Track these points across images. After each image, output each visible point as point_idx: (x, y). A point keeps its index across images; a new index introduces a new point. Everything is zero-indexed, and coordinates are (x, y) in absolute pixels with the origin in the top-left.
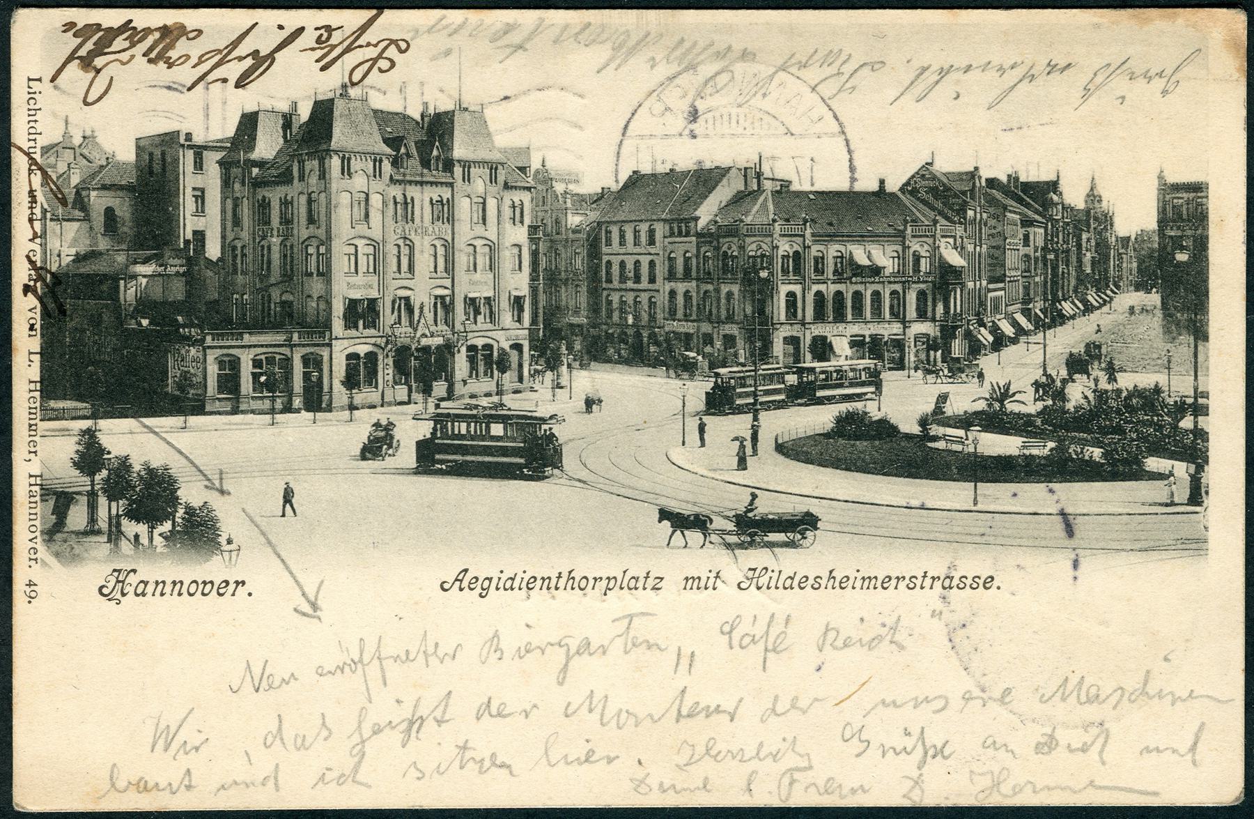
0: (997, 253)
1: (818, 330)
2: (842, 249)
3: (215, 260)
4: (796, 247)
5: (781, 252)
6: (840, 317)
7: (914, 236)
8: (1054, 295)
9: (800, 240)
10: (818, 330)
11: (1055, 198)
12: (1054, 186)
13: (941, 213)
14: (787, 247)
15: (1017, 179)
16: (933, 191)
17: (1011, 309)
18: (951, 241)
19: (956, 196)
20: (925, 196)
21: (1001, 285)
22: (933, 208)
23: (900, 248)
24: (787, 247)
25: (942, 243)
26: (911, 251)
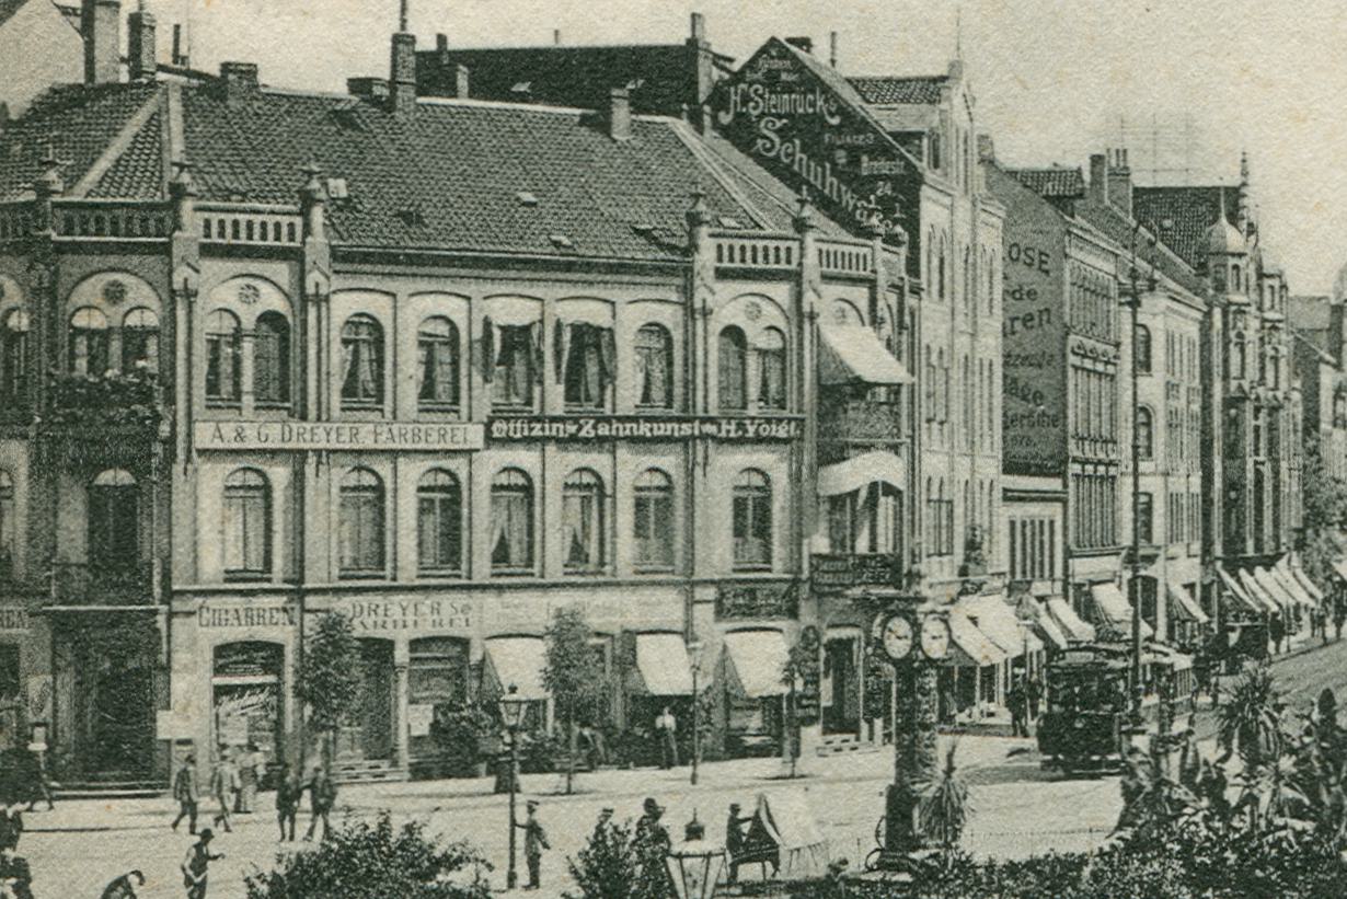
0: (1038, 379)
1: (445, 614)
2: (454, 308)
3: (803, 729)
4: (273, 300)
5: (209, 324)
6: (514, 564)
7: (722, 274)
8: (1233, 542)
9: (281, 271)
10: (445, 614)
11: (1234, 238)
12: (1229, 201)
13: (827, 205)
14: (228, 295)
15: (1123, 174)
16: (803, 128)
17: (1083, 568)
18: (860, 295)
19: (882, 150)
20: (780, 148)
21: (1054, 484)
22: (792, 179)
23: (669, 316)
24: (228, 295)
25: (825, 299)
26: (716, 326)
